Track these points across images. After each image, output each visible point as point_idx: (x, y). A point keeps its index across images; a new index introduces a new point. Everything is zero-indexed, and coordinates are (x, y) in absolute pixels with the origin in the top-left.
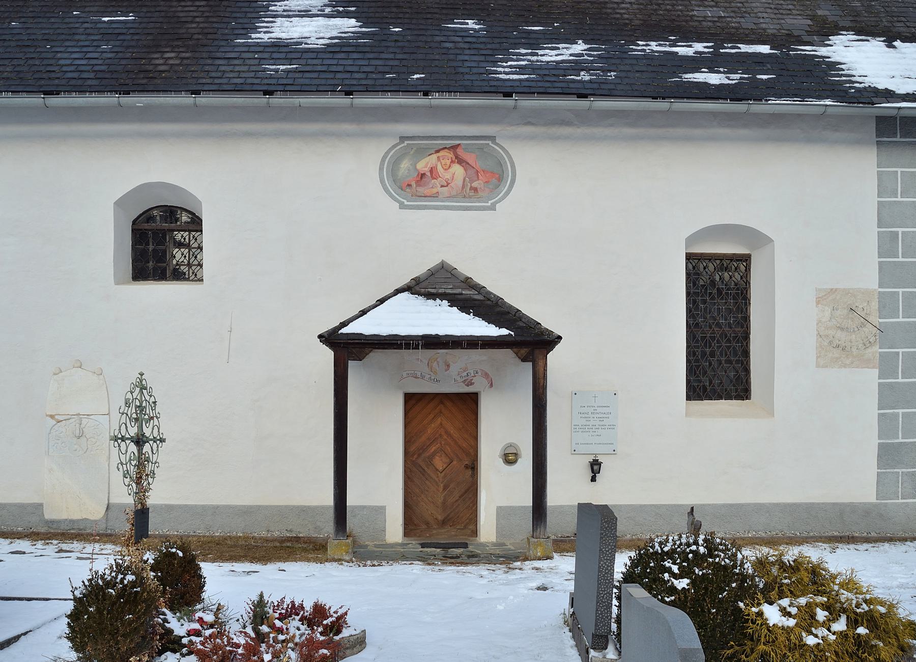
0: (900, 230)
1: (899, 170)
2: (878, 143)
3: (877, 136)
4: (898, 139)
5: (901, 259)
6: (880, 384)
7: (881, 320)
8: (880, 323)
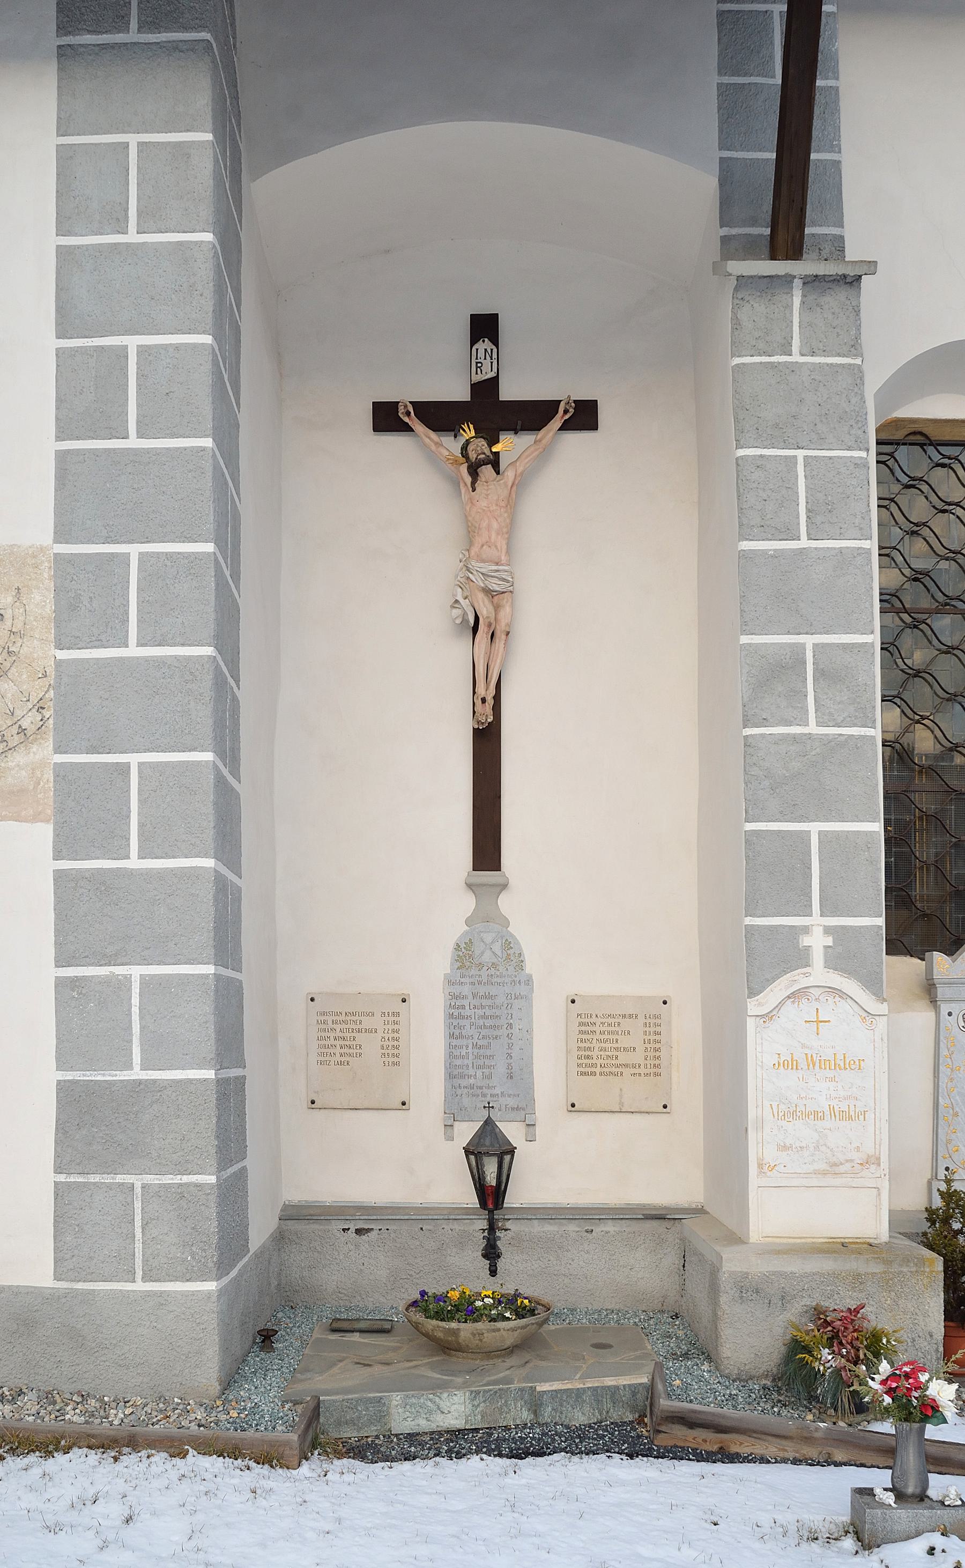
0: (132, 342)
1: (133, 140)
2: (63, 53)
3: (62, 29)
4: (133, 35)
5: (133, 442)
6: (59, 876)
7: (63, 655)
8: (59, 664)
